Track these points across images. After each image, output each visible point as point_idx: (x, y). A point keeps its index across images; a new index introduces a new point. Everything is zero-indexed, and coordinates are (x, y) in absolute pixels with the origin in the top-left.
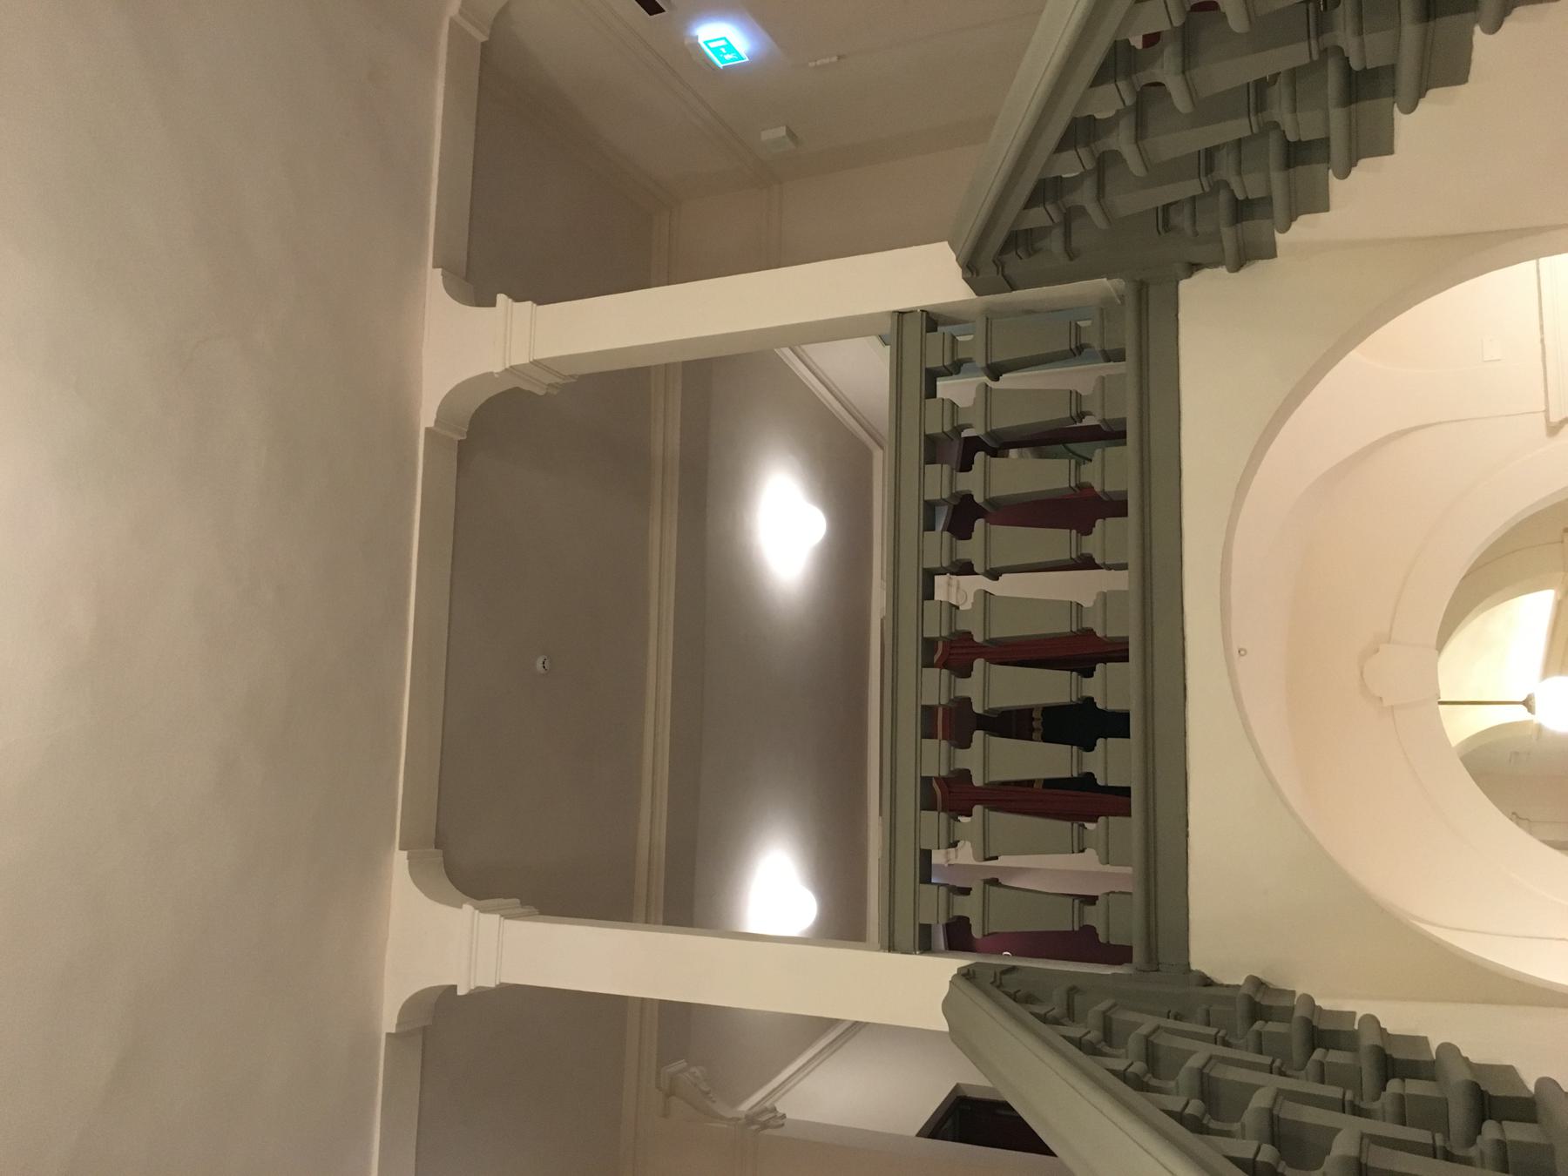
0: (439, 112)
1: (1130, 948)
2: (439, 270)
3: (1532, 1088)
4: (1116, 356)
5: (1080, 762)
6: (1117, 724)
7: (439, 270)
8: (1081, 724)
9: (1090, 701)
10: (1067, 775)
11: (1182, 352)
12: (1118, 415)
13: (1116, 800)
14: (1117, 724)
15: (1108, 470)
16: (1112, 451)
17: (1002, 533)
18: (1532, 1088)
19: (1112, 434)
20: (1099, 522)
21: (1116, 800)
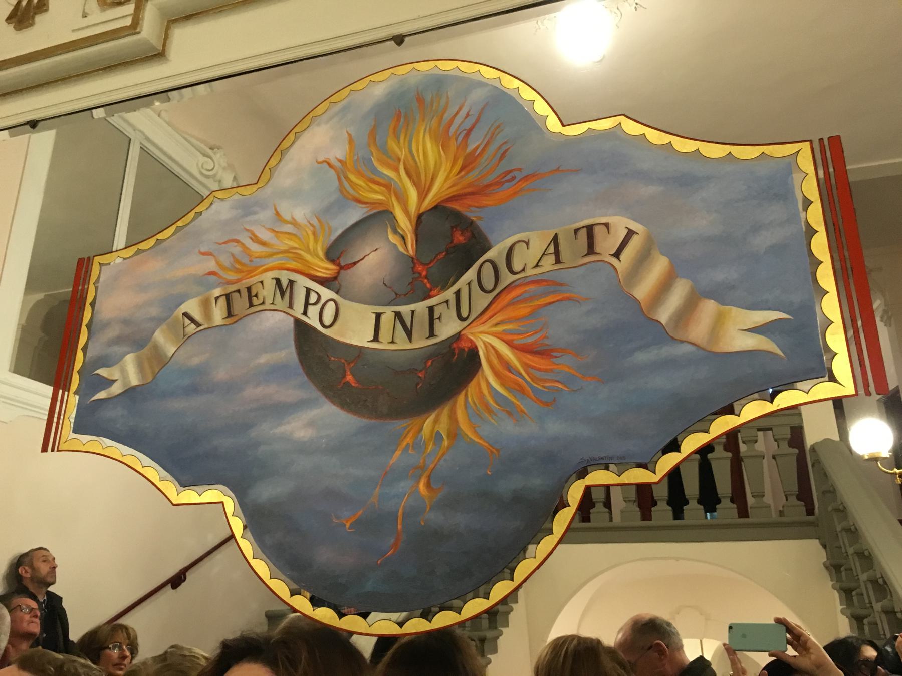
0: (865, 165)
1: (650, 519)
2: (77, 397)
3: (489, 656)
4: (781, 513)
5: (662, 500)
6: (678, 514)
7: (77, 397)
8: (709, 499)
9: (687, 502)
10: (719, 491)
11: (782, 542)
12: (685, 517)
13: (646, 515)
14: (678, 514)
15: (726, 509)
16: (735, 512)
17: (728, 464)
18: (489, 656)
19: (743, 512)
20: (803, 503)
21: (646, 515)
